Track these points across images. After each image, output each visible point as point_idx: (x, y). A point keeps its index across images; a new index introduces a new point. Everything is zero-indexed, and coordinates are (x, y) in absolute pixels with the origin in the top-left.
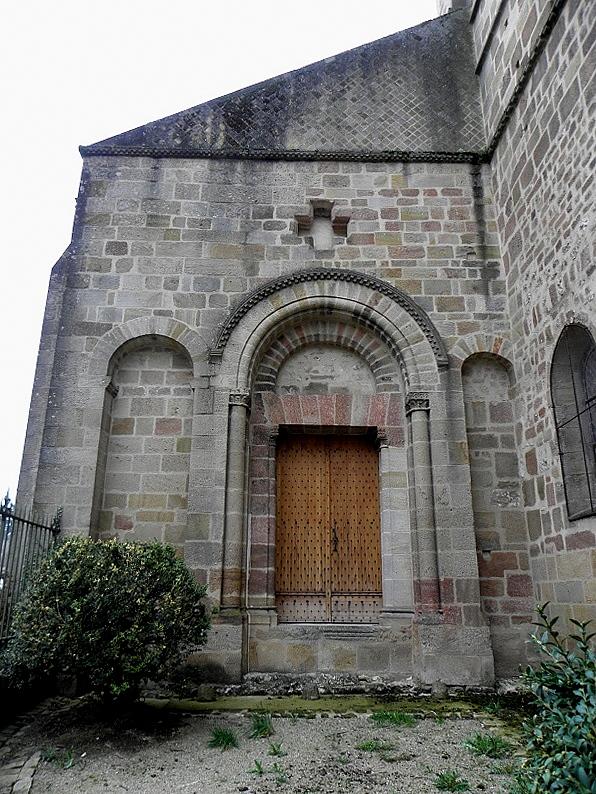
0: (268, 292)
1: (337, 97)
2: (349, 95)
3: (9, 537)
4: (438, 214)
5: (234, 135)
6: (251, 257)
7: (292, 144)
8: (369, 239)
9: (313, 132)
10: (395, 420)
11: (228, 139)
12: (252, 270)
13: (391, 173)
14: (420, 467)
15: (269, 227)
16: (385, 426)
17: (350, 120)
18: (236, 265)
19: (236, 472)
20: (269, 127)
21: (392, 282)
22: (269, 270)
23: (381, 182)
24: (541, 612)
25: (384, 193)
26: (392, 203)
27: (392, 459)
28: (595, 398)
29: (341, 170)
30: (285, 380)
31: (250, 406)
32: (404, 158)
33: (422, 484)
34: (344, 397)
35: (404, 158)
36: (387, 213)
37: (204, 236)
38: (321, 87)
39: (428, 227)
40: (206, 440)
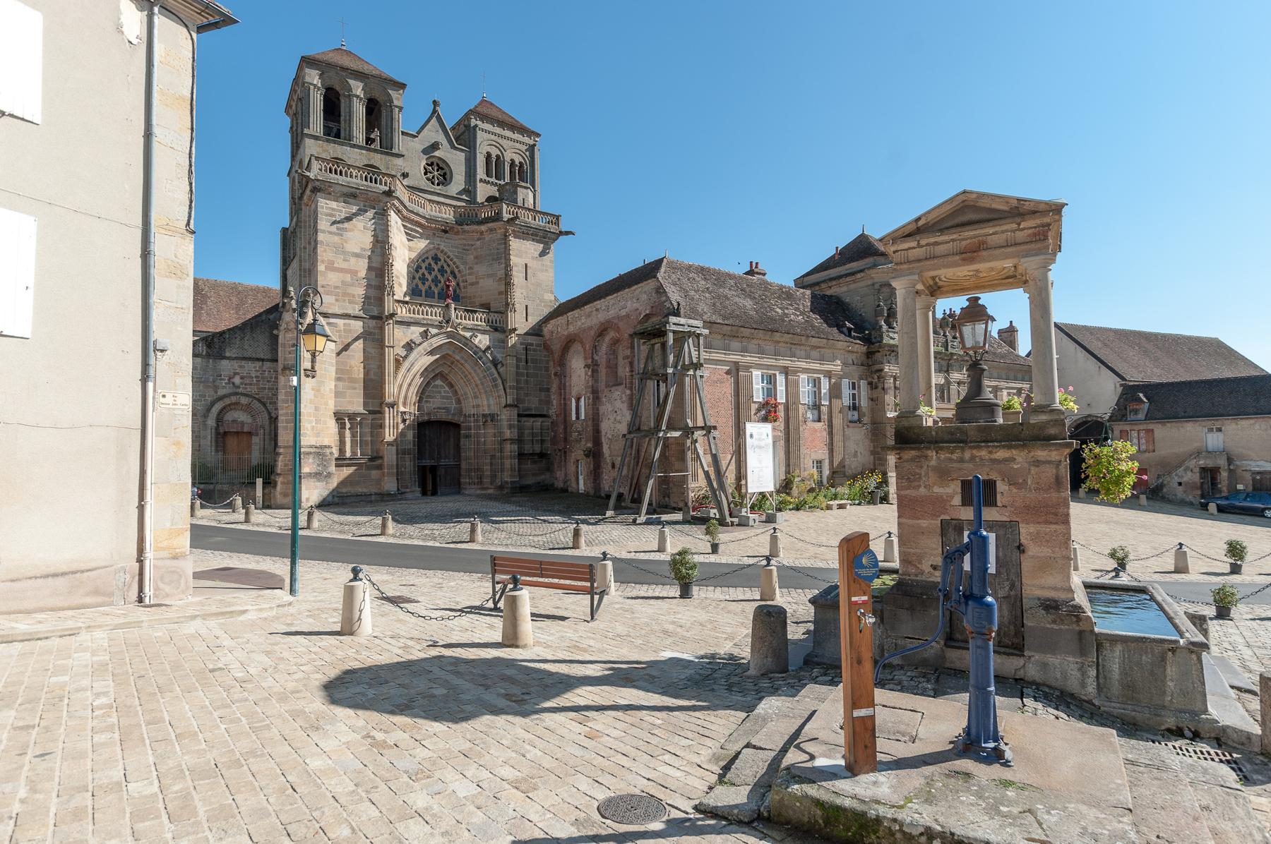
0: (221, 398)
1: (242, 339)
2: (246, 338)
3: (625, 468)
4: (271, 378)
5: (209, 350)
6: (216, 388)
7: (228, 354)
8: (251, 384)
9: (234, 350)
10: (256, 430)
11: (207, 352)
12: (216, 392)
13: (258, 364)
14: (262, 442)
15: (221, 380)
16: (317, 704)
17: (246, 347)
18: (212, 393)
19: (213, 444)
20: (220, 348)
21: (257, 396)
22: (221, 392)
23: (255, 367)
24: (1029, 811)
25: (256, 371)
26: (258, 374)
27: (255, 440)
28: (2, 643)
29: (243, 363)
30: (225, 419)
31: (217, 428)
32: (263, 360)
33: (262, 446)
34: (243, 423)
35: (263, 360)
36: (257, 377)
37: (201, 382)
38: (237, 336)
39: (268, 381)
40: (205, 438)
